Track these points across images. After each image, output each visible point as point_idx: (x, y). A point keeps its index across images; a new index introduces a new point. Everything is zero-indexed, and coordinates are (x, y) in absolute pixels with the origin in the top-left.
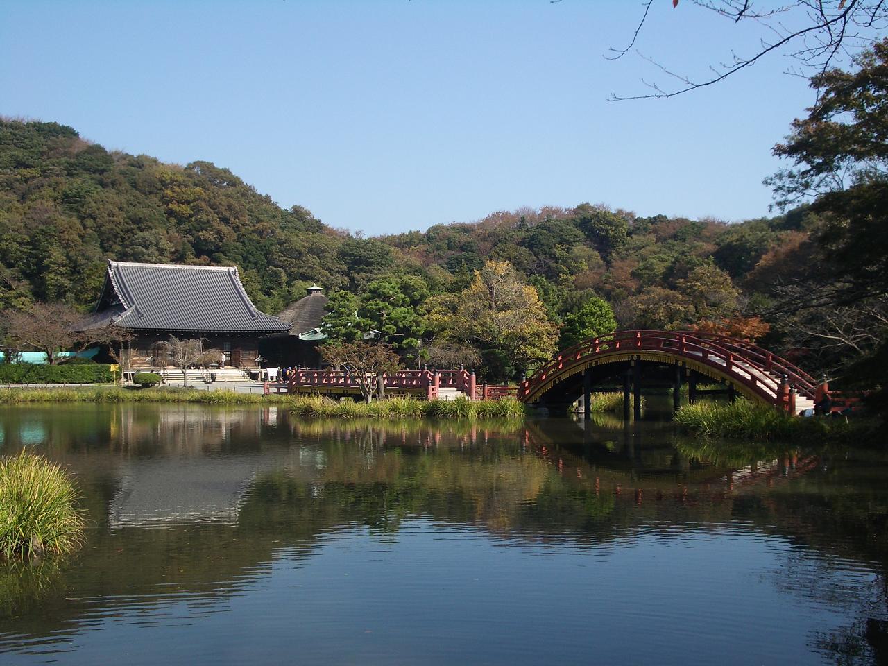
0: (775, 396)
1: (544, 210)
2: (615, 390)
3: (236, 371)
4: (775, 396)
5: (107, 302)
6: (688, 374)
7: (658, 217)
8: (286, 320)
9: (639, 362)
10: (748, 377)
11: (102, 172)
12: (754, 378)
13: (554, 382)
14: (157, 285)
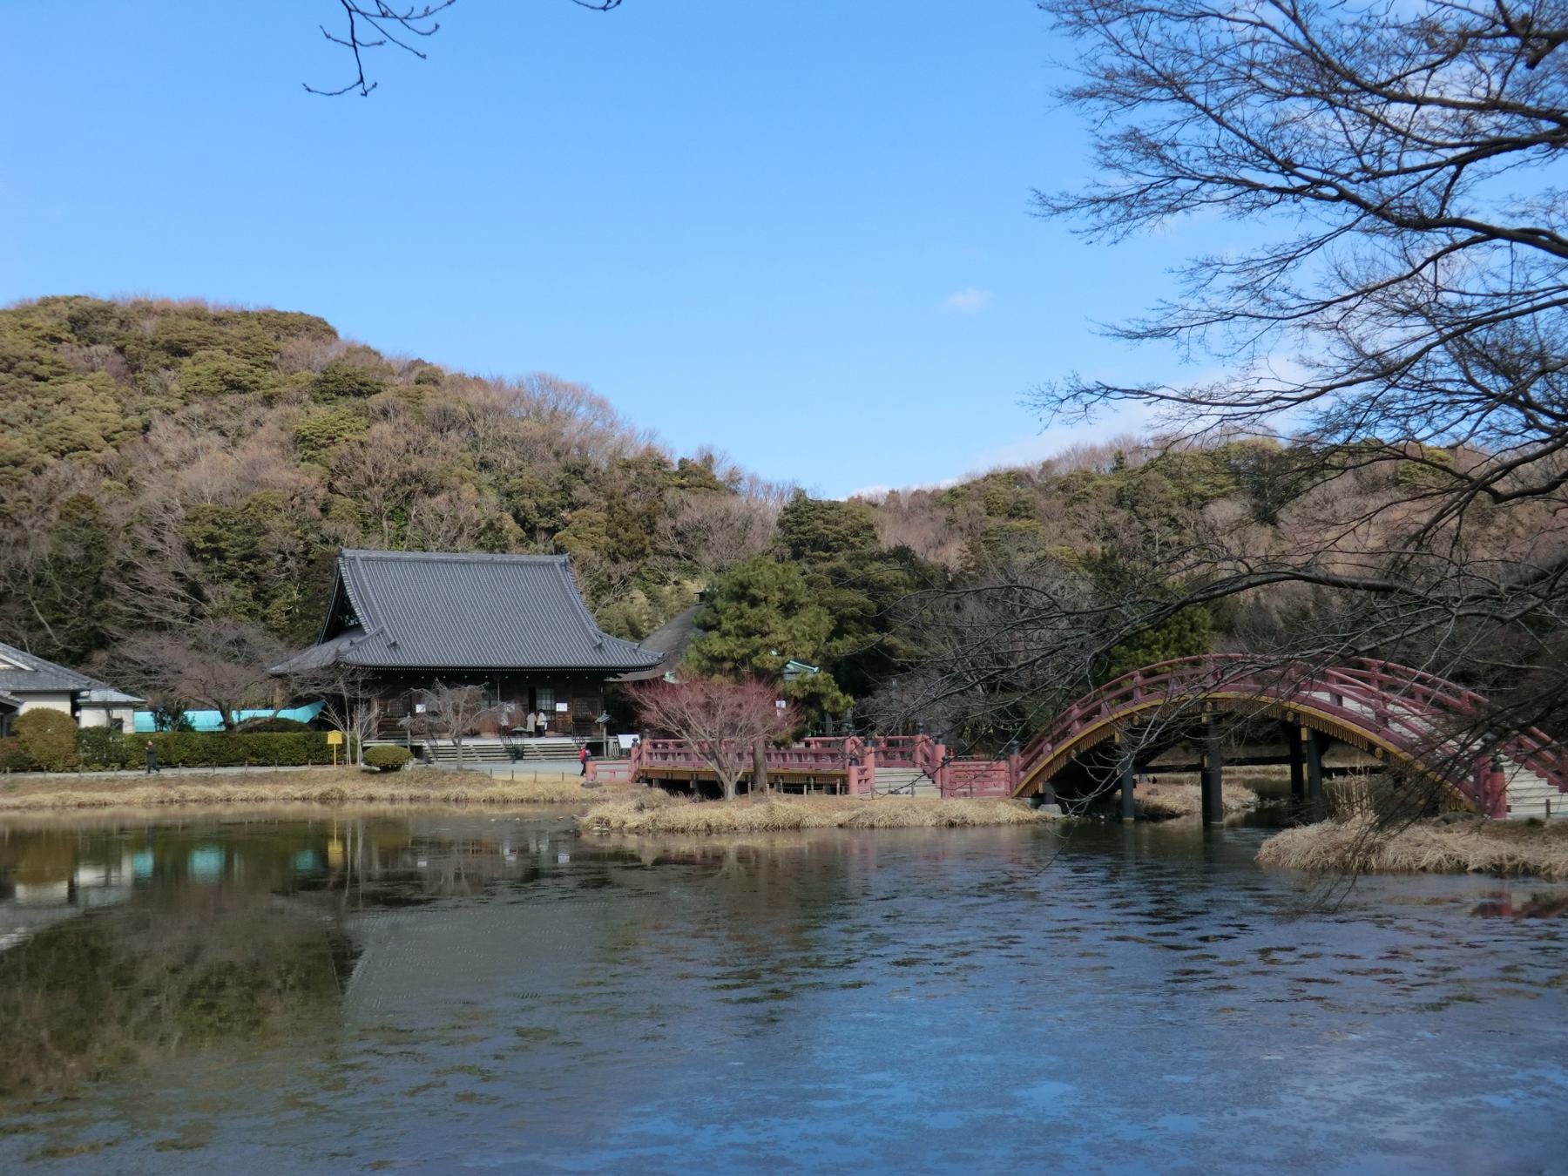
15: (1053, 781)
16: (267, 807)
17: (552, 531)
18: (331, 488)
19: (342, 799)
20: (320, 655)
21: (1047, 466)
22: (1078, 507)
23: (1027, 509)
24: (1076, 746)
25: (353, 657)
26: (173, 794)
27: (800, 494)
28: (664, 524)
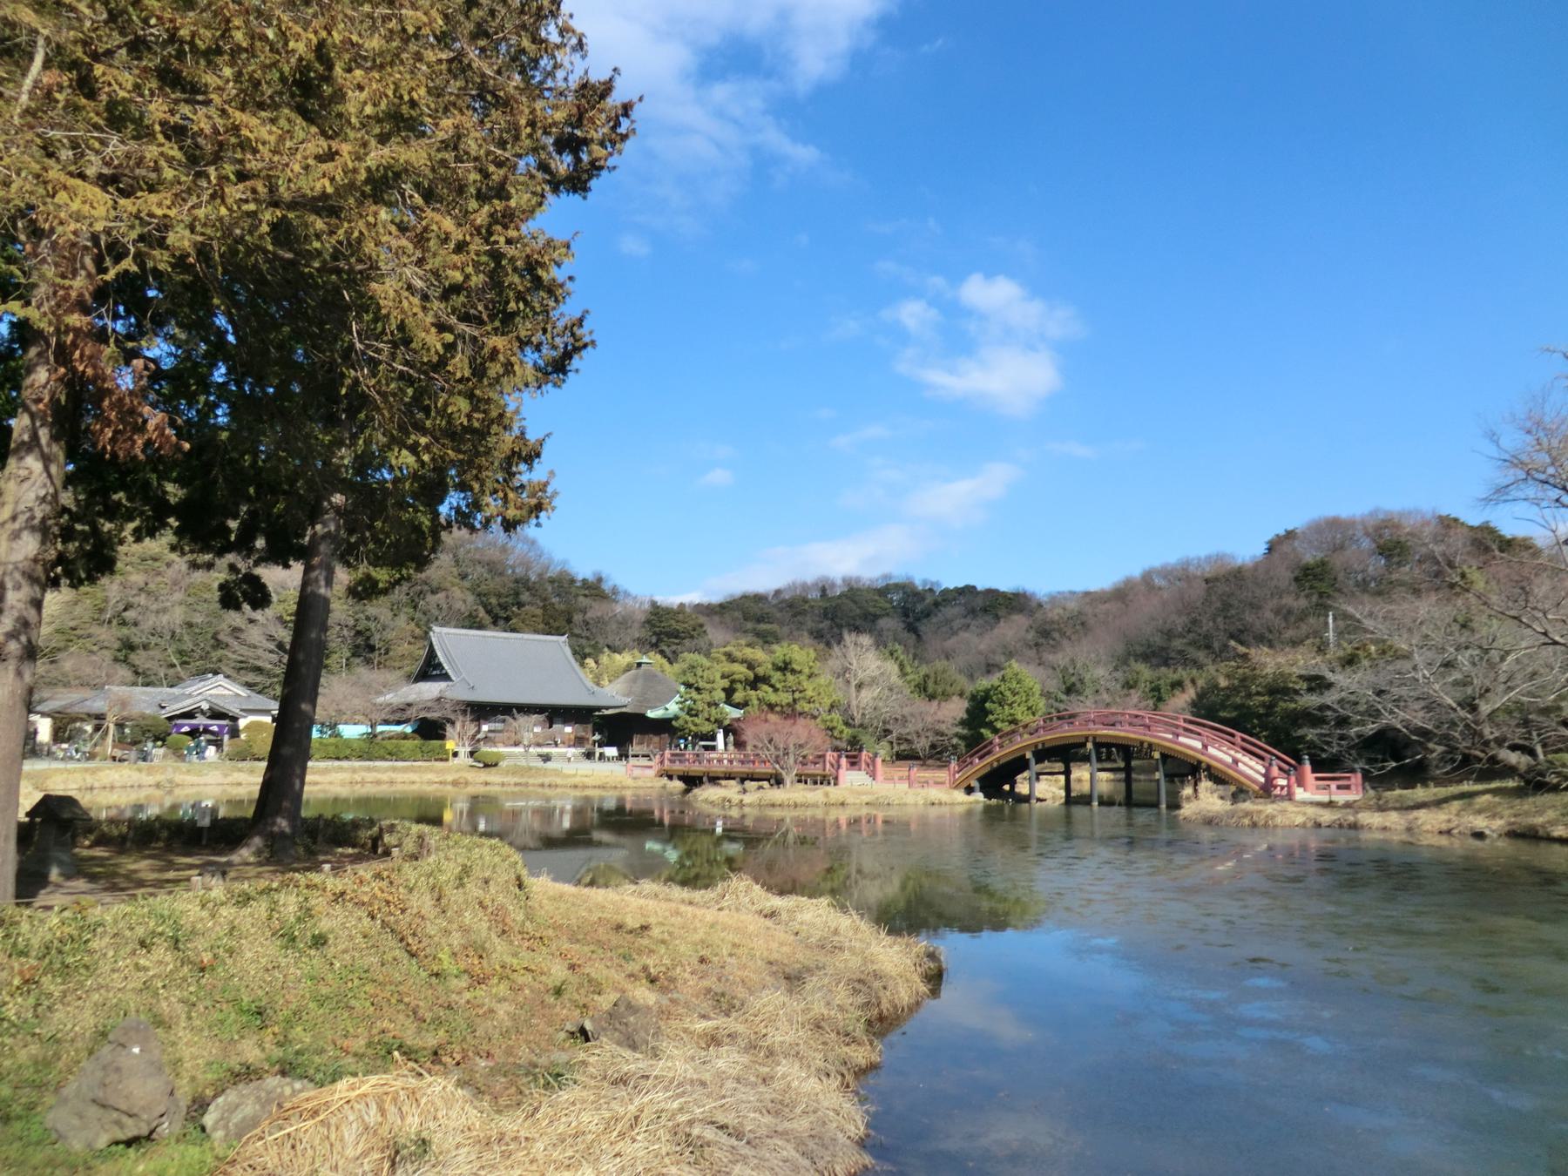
1: (844, 580)
5: (430, 669)
8: (614, 695)
10: (1229, 760)
12: (1236, 761)
15: (980, 780)
16: (415, 787)
17: (507, 619)
19: (467, 783)
20: (429, 690)
21: (778, 592)
22: (799, 618)
24: (998, 760)
25: (448, 695)
26: (358, 777)
27: (654, 604)
28: (577, 618)
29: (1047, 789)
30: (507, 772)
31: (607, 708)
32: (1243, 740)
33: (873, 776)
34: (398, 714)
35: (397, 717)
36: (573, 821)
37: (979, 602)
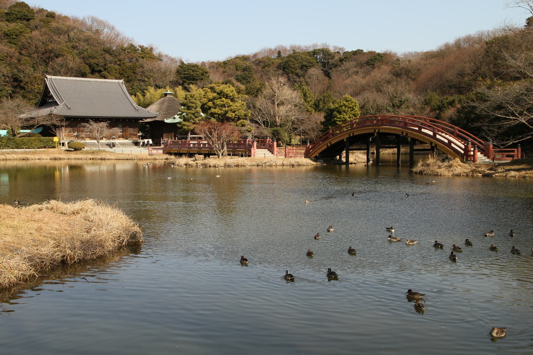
0: (463, 152)
1: (291, 47)
2: (393, 147)
3: (127, 141)
4: (463, 152)
5: (46, 99)
6: (409, 140)
7: (358, 50)
8: (153, 112)
9: (379, 133)
10: (446, 141)
11: (28, 20)
12: (450, 142)
13: (327, 145)
14: (74, 93)
18: (20, 53)
20: (45, 111)
21: (255, 55)
23: (249, 69)
28: (138, 70)
29: (358, 158)
30: (87, 153)
31: (146, 118)
32: (459, 131)
33: (272, 152)
34: (28, 124)
35: (26, 124)
36: (93, 174)
37: (365, 59)
